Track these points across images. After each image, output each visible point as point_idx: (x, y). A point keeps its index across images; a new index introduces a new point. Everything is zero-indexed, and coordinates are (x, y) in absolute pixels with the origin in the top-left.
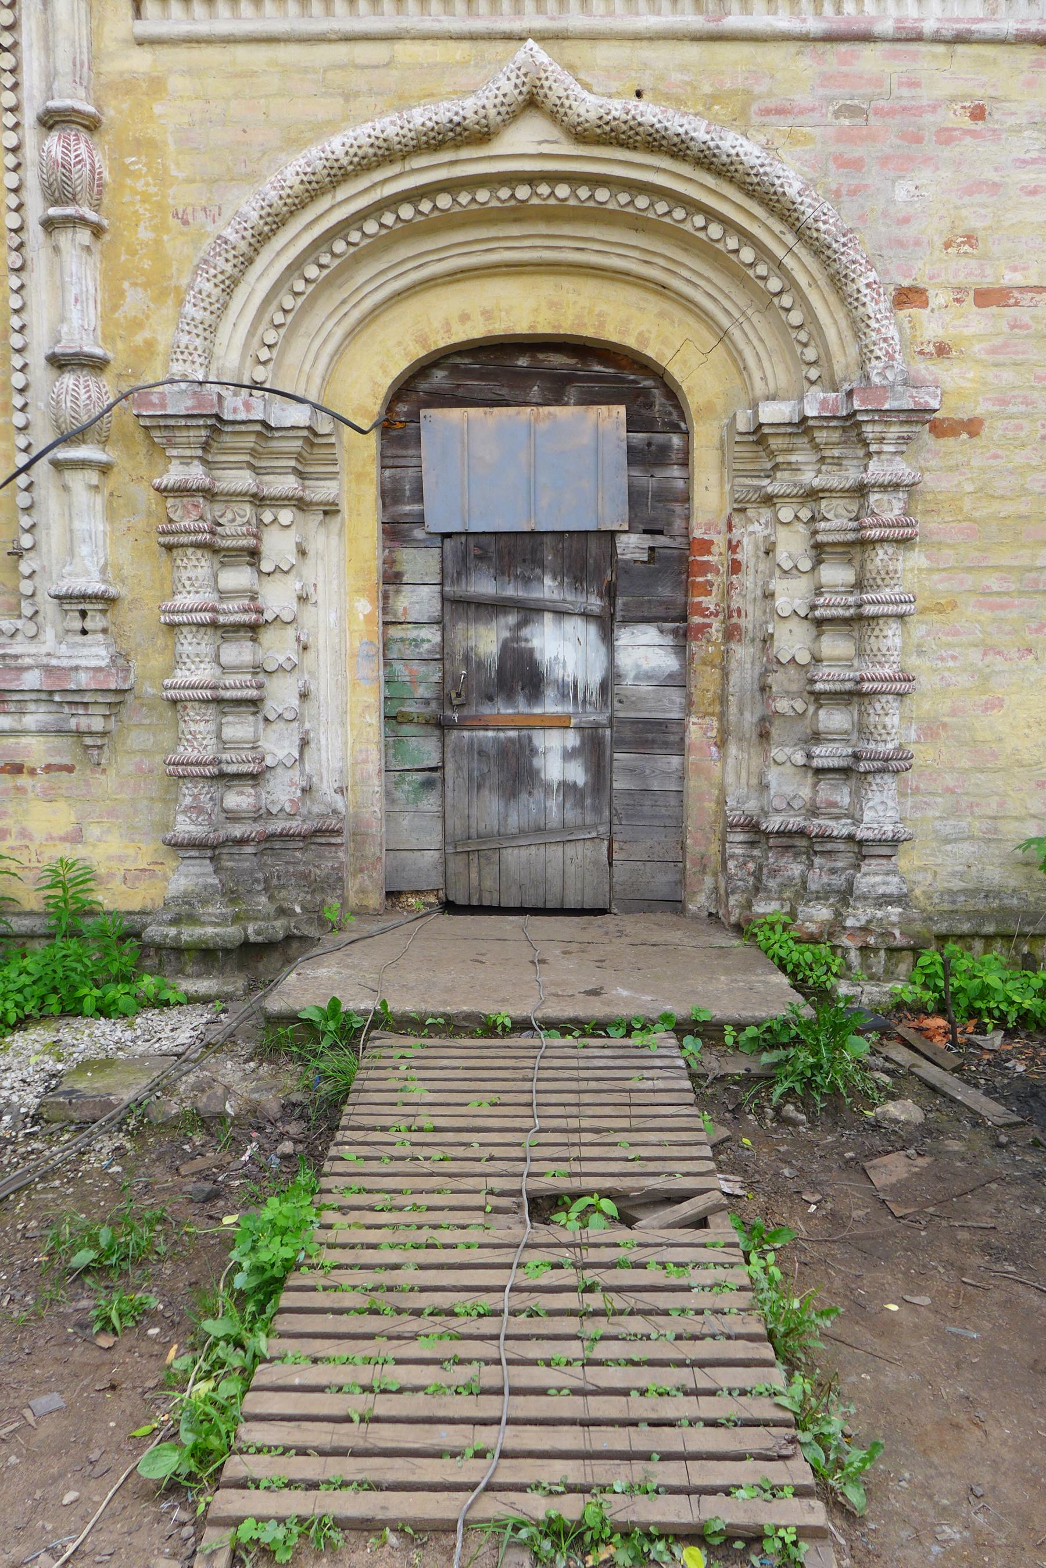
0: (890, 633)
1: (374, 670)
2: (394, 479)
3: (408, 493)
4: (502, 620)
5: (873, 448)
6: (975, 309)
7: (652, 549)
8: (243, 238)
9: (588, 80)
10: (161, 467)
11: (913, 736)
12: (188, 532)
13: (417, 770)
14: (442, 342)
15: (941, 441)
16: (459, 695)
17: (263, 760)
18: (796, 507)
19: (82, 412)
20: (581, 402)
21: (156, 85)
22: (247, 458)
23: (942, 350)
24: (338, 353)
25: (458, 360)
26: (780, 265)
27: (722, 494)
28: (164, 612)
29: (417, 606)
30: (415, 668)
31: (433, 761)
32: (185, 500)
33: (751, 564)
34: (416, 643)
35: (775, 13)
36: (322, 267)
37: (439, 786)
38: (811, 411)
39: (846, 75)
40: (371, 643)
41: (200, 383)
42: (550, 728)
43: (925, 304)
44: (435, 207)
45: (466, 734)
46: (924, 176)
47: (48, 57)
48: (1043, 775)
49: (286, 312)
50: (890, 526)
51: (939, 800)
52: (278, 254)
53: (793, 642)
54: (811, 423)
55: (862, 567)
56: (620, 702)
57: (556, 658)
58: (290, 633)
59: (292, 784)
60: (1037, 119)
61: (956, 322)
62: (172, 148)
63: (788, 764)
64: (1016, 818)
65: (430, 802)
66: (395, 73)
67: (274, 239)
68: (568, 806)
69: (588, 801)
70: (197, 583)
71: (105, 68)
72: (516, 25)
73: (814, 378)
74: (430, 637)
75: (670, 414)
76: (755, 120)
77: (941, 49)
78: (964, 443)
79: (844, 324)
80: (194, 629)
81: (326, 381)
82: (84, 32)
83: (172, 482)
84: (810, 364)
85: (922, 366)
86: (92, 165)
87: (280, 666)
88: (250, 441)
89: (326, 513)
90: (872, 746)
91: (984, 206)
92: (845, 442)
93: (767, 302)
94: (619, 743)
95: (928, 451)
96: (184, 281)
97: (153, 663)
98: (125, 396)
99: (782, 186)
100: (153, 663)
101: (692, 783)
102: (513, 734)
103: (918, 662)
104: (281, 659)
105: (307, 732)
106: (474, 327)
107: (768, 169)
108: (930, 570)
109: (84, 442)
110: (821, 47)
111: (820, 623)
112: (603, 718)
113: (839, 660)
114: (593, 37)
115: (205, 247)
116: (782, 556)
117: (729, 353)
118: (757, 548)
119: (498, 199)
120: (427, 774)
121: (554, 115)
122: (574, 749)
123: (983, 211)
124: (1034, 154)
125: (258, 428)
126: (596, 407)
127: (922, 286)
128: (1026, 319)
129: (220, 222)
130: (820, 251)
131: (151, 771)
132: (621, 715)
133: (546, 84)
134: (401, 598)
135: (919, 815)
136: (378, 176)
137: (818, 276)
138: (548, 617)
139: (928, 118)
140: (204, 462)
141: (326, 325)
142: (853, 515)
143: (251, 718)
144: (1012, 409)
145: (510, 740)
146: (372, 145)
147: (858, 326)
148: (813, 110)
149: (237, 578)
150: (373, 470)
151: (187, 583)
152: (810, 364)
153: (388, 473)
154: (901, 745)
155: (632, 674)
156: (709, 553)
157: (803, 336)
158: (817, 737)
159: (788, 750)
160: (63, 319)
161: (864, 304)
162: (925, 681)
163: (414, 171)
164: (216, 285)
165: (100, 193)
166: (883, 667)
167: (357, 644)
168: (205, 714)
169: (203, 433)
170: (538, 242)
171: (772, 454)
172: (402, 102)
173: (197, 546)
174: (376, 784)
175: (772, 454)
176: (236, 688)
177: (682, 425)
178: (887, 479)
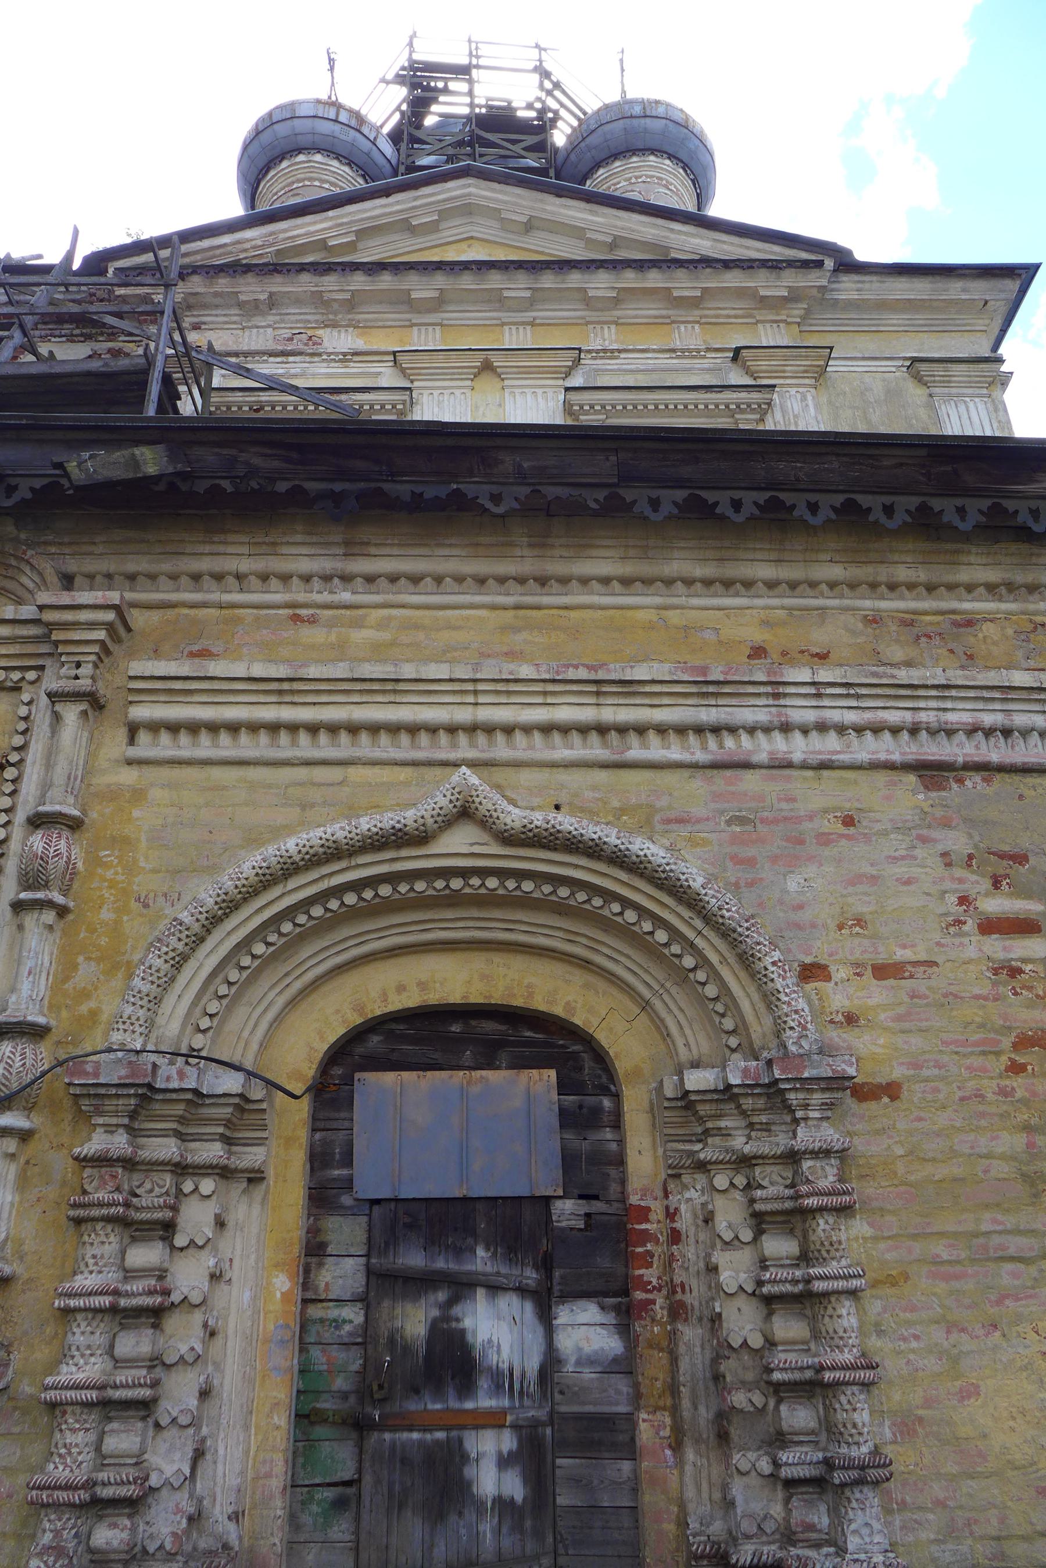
0: (844, 1312)
1: (287, 1359)
2: (324, 1142)
3: (337, 1157)
4: (432, 1298)
5: (799, 1114)
6: (875, 982)
7: (588, 1215)
8: (198, 920)
9: (514, 796)
10: (84, 1134)
11: (888, 1434)
12: (101, 1205)
13: (329, 1485)
14: (378, 1010)
15: (864, 1105)
16: (381, 1387)
17: (147, 1478)
18: (731, 1174)
19: (14, 1079)
20: (508, 1068)
21: (138, 795)
22: (174, 1125)
23: (851, 1019)
24: (278, 1019)
25: (394, 1026)
26: (692, 945)
27: (656, 1157)
28: (61, 1295)
29: (340, 1281)
30: (334, 1354)
31: (348, 1475)
32: (104, 1170)
33: (691, 1233)
34: (337, 1323)
35: (669, 748)
36: (268, 944)
37: (354, 1505)
38: (735, 1080)
39: (733, 793)
40: (287, 1326)
41: (137, 1052)
42: (484, 1427)
43: (828, 978)
44: (377, 895)
45: (387, 1436)
46: (811, 871)
47: (47, 770)
48: (1040, 1478)
49: (230, 984)
50: (826, 1195)
51: (931, 1517)
52: (229, 934)
53: (742, 1323)
54: (736, 1090)
55: (805, 1237)
56: (561, 1393)
57: (490, 1341)
58: (198, 1317)
59: (178, 1510)
60: (900, 825)
61: (859, 994)
62: (143, 844)
63: (753, 1473)
64: (1024, 1538)
65: (341, 1530)
66: (347, 789)
67: (226, 921)
68: (505, 1530)
69: (528, 1523)
70: (100, 1266)
71: (95, 781)
72: (452, 756)
73: (734, 1046)
74: (352, 1316)
75: (600, 1077)
76: (659, 827)
77: (810, 773)
78: (886, 1106)
79: (756, 997)
80: (90, 1316)
81: (263, 1046)
82: (83, 754)
83: (92, 1151)
84: (729, 1033)
85: (834, 1034)
86: (69, 858)
87: (182, 1357)
88: (179, 1109)
89: (250, 1180)
90: (844, 1450)
91: (866, 894)
92: (771, 1108)
93: (683, 976)
94: (562, 1445)
95: (853, 1115)
96: (137, 957)
97: (38, 1355)
98: (60, 1064)
99: (687, 880)
100: (38, 1355)
101: (647, 1498)
102: (440, 1435)
103: (879, 1344)
104: (184, 1349)
105: (203, 1440)
106: (409, 997)
107: (673, 867)
108: (875, 1239)
109: (9, 1109)
110: (710, 773)
111: (769, 1301)
112: (542, 1414)
113: (794, 1343)
114: (517, 764)
115: (161, 927)
116: (721, 1225)
117: (652, 1021)
118: (695, 1216)
119: (435, 889)
120: (340, 1490)
121: (485, 823)
122: (510, 1453)
123: (867, 899)
124: (903, 853)
125: (189, 1096)
126: (526, 1071)
127: (823, 962)
128: (923, 990)
129: (178, 906)
130: (726, 933)
131: (10, 1496)
132: (563, 1409)
133: (477, 800)
134: (324, 1272)
135: (911, 1538)
136: (326, 870)
137: (727, 955)
138: (481, 1293)
139: (807, 825)
140: (130, 1129)
141: (269, 995)
142: (789, 1182)
143: (140, 1425)
144: (926, 1073)
145: (437, 1442)
146: (322, 846)
147: (770, 999)
148: (707, 819)
149: (145, 1255)
150: (303, 1134)
151: (91, 1261)
152: (729, 1033)
153: (318, 1136)
154: (876, 1446)
155: (573, 1360)
156: (647, 1221)
157: (720, 1008)
158: (780, 1439)
159: (752, 1455)
160: (13, 990)
161: (772, 980)
162: (892, 1367)
163: (358, 866)
164: (166, 961)
165: (71, 880)
166: (842, 1351)
167: (271, 1327)
168: (85, 1421)
169: (133, 1101)
170: (471, 924)
171: (701, 1120)
172: (351, 811)
173: (108, 1219)
174: (278, 1507)
175: (701, 1120)
176: (127, 1386)
177: (612, 1087)
178: (817, 1145)
